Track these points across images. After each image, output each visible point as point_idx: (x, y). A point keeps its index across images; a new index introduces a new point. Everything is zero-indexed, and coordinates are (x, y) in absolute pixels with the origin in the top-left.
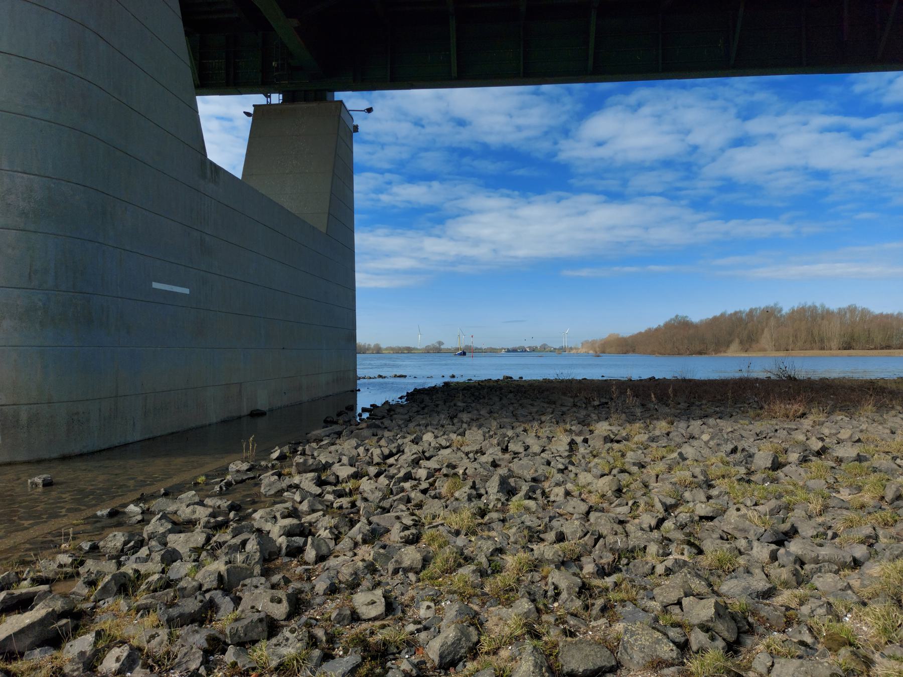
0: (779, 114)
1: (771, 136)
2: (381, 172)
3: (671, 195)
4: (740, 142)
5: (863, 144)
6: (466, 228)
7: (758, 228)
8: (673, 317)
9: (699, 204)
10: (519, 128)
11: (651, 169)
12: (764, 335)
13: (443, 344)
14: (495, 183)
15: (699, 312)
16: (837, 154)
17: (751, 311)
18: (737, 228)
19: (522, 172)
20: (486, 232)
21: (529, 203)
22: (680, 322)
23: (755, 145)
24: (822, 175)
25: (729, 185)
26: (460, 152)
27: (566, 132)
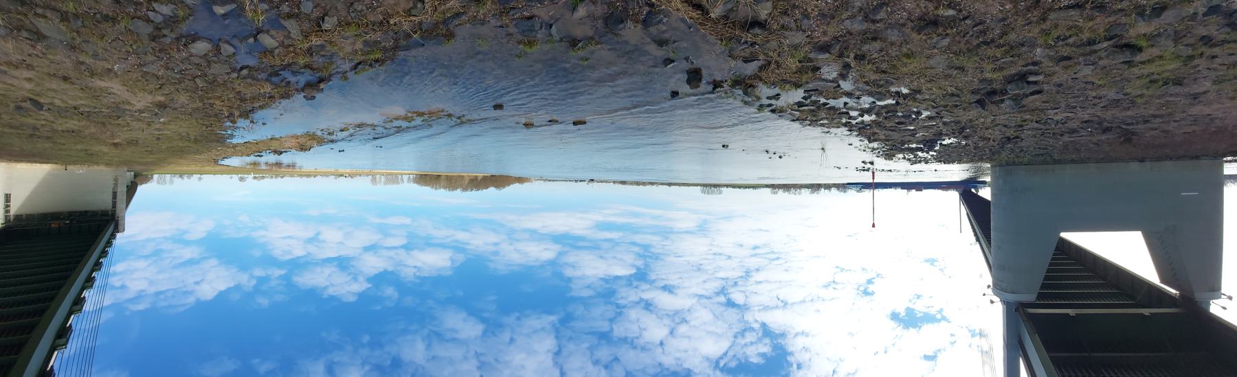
4: (496, 244)
14: (582, 239)
15: (492, 190)
25: (494, 231)
27: (560, 254)
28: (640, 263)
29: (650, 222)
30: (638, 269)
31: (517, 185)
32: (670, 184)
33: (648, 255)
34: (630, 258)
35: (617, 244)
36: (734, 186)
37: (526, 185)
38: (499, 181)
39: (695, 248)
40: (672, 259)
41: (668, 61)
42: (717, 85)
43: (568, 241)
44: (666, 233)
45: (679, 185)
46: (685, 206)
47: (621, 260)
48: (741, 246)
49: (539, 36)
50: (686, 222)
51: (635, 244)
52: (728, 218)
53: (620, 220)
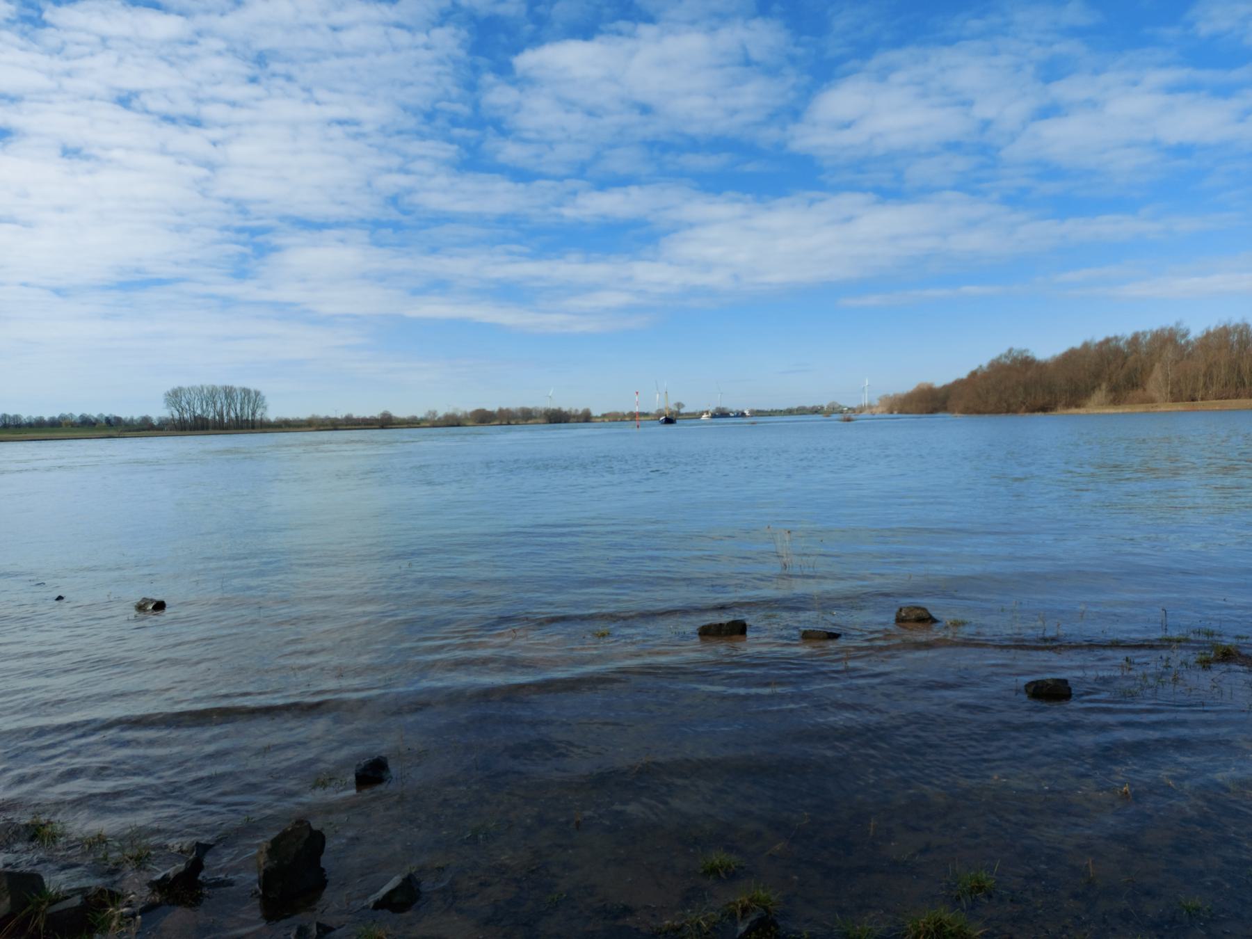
0: (1097, 72)
1: (1092, 104)
2: (560, 179)
3: (969, 186)
4: (1050, 111)
5: (1236, 104)
7: (1108, 227)
9: (1016, 200)
10: (734, 112)
11: (931, 154)
12: (1154, 375)
13: (683, 406)
14: (712, 184)
16: (1199, 121)
17: (1135, 339)
18: (1078, 229)
19: (751, 167)
22: (1015, 360)
23: (1067, 115)
24: (1183, 150)
25: (1050, 171)
27: (795, 114)
28: (499, 96)
29: (459, 266)
30: (504, 70)
32: (386, 422)
33: (470, 134)
34: (539, 113)
35: (580, 170)
36: (113, 428)
37: (906, 384)
38: (1016, 390)
39: (285, 154)
42: (185, 888)
43: (762, 169)
44: (396, 224)
46: (325, 337)
47: (569, 105)
50: (324, 270)
51: (520, 175)
52: (133, 284)
53: (569, 268)
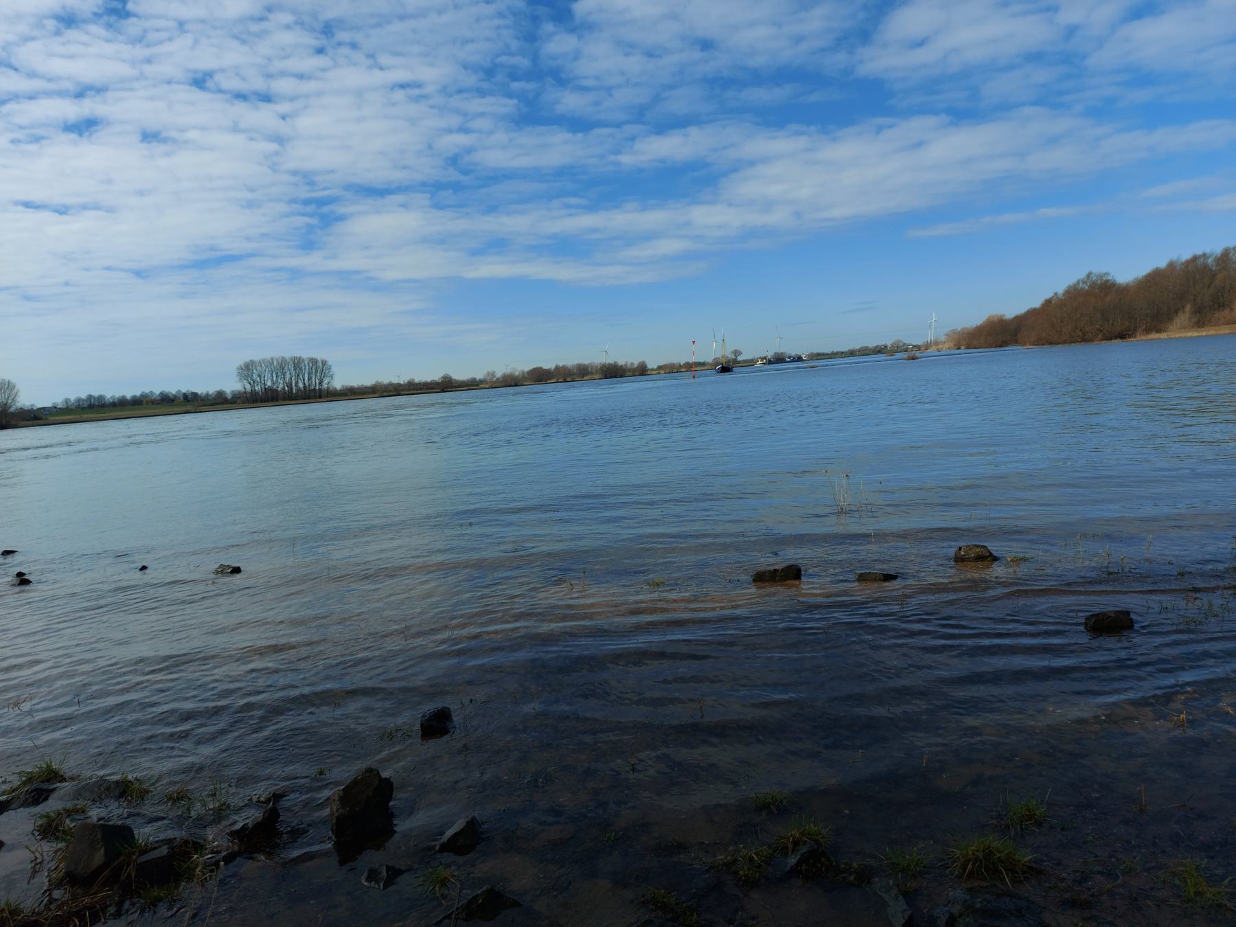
2: (618, 125)
3: (1050, 100)
6: (748, 187)
8: (1082, 276)
9: (1101, 112)
10: (799, 39)
11: (1010, 67)
13: (740, 353)
14: (775, 119)
15: (1127, 269)
18: (1169, 139)
19: (814, 98)
20: (774, 190)
21: (834, 139)
22: (1094, 284)
25: (1141, 77)
26: (718, 83)
28: (558, 44)
31: (1012, 310)
32: (446, 386)
37: (974, 318)
38: (1096, 316)
40: (431, 74)
41: (469, 840)
44: (456, 185)
45: (413, 388)
48: (149, 136)
49: (958, 893)
50: (387, 235)
51: (578, 125)
52: (208, 263)
